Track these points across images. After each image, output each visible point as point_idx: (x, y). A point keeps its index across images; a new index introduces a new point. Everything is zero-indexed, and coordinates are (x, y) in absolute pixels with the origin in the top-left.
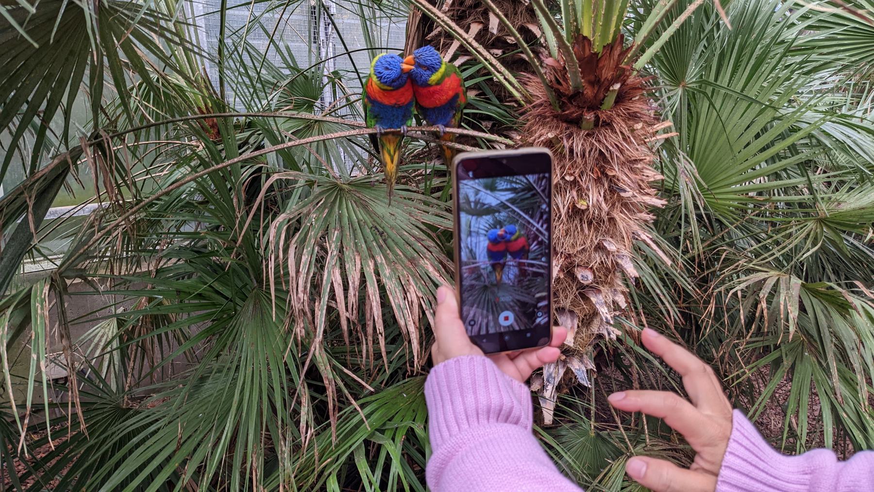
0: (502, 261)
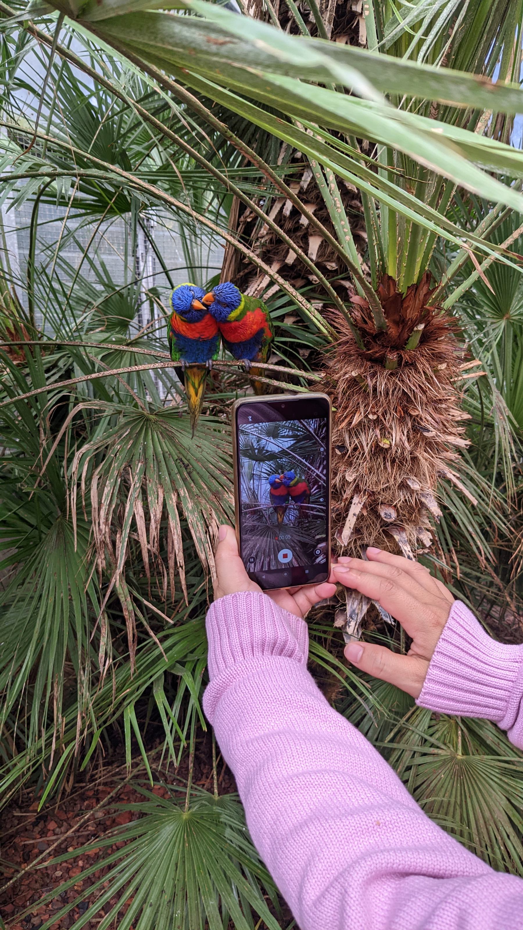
0: (284, 505)
